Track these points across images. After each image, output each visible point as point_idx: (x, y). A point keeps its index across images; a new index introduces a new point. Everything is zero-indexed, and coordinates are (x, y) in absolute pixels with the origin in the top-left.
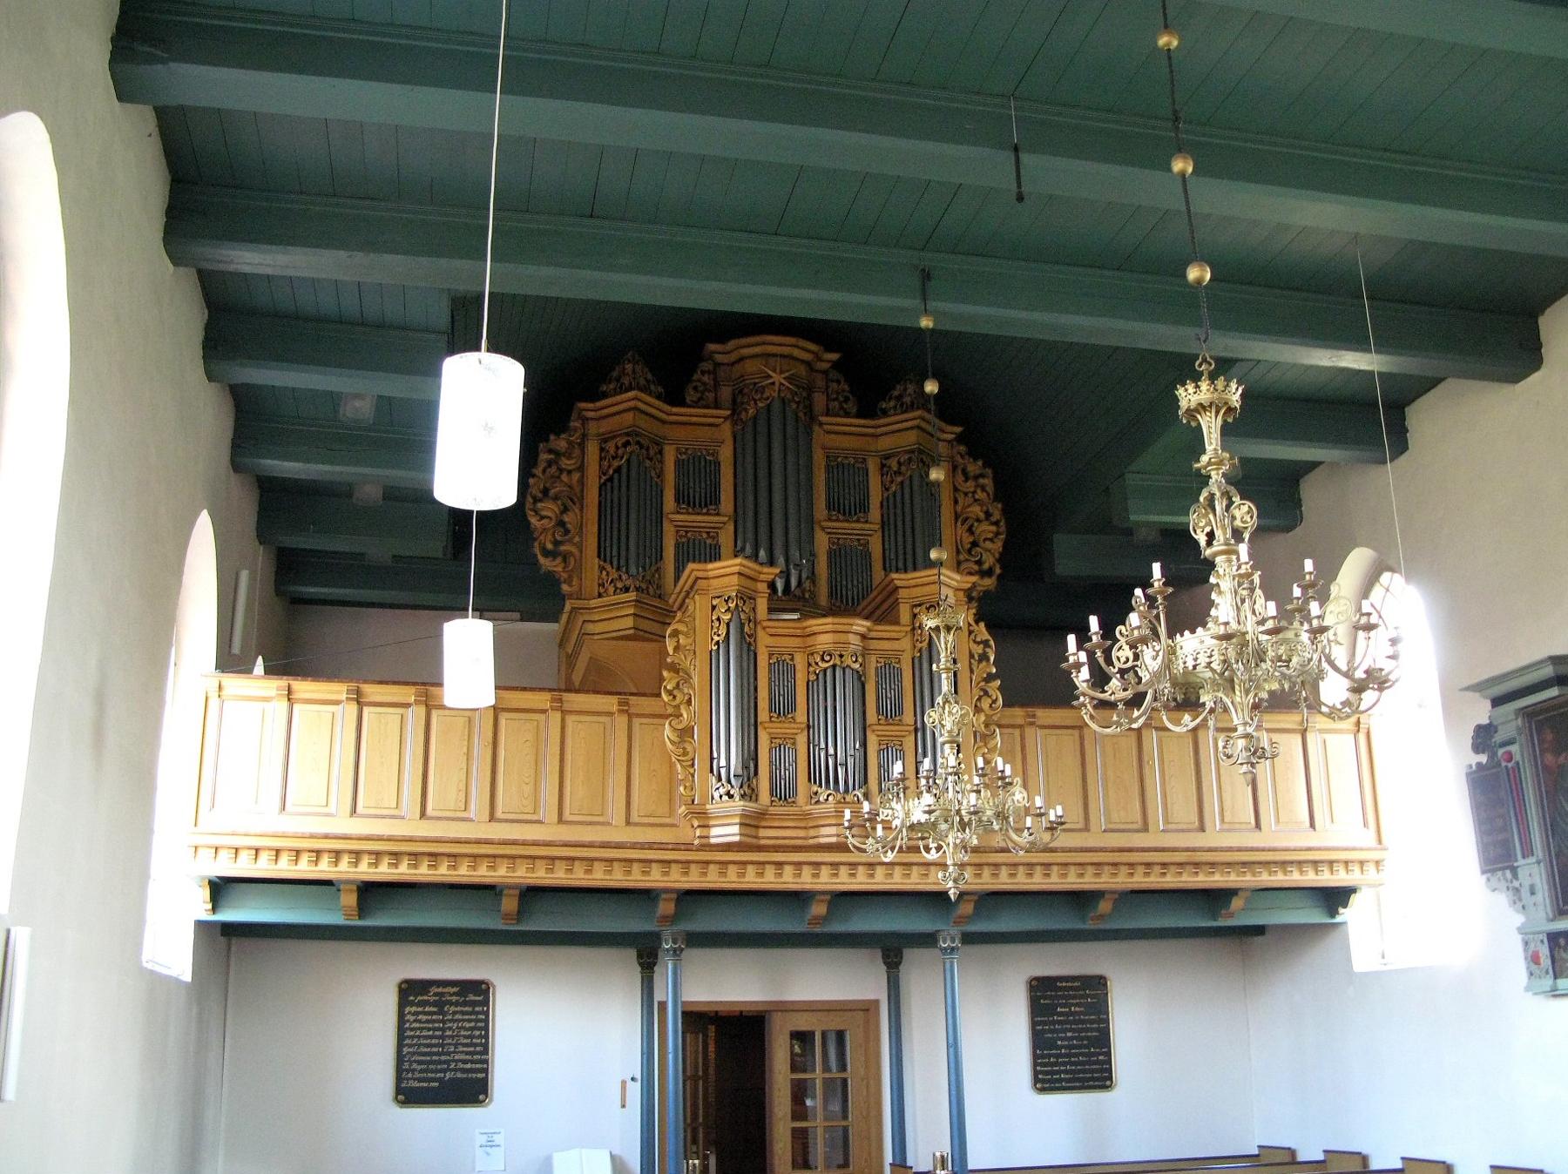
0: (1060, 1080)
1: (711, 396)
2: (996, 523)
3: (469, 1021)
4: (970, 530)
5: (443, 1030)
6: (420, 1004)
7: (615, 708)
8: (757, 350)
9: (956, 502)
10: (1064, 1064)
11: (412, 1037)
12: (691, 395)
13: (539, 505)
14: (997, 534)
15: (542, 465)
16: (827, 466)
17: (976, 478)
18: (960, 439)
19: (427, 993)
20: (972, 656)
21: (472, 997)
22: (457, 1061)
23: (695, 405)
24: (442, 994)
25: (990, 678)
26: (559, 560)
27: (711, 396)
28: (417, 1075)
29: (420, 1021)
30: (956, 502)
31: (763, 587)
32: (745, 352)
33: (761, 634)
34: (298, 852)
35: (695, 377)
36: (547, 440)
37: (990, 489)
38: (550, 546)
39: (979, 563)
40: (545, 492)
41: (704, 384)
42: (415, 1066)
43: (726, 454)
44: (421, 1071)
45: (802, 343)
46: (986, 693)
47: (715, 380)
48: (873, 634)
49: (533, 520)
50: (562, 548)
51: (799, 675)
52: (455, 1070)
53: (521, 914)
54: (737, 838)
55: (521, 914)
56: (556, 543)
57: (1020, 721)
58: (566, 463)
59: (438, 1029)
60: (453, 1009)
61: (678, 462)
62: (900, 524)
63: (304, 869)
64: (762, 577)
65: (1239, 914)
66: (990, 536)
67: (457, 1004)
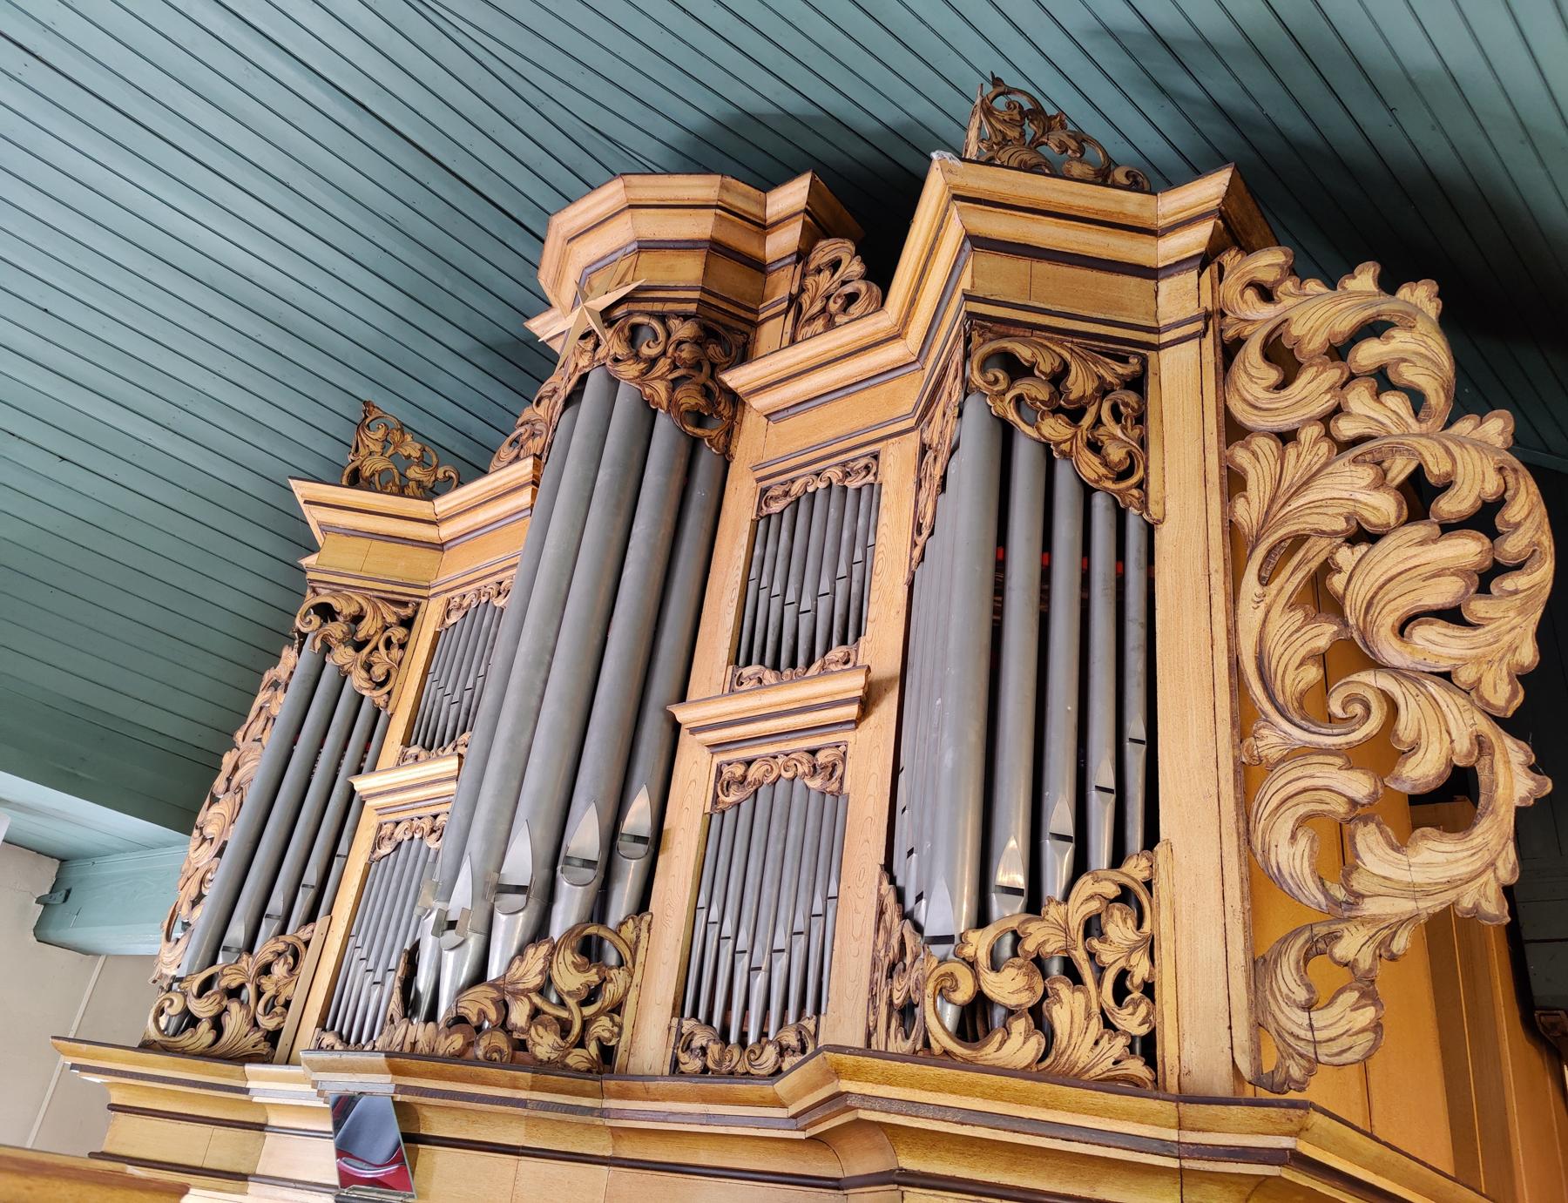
4: (1319, 596)
9: (1234, 482)
14: (1486, 578)
17: (1338, 351)
30: (1234, 482)
39: (1383, 753)
62: (393, 885)
66: (1443, 593)
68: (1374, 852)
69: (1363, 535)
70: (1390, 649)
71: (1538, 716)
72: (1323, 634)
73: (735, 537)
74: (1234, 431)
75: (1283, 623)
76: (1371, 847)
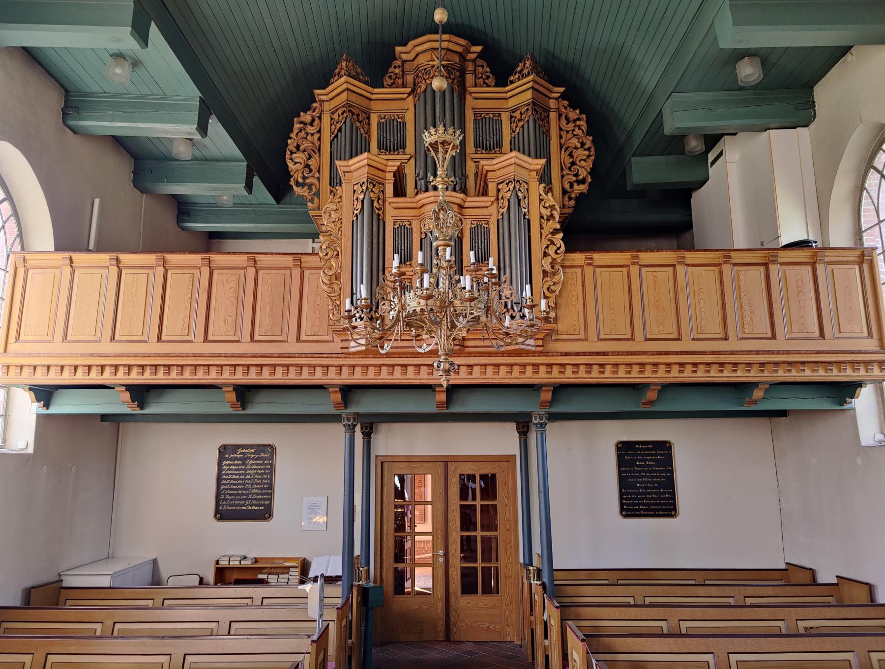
0: (639, 510)
1: (400, 81)
2: (589, 149)
3: (261, 469)
4: (571, 155)
5: (245, 475)
6: (231, 459)
7: (291, 264)
8: (425, 46)
9: (561, 137)
10: (642, 499)
11: (226, 480)
12: (387, 81)
13: (294, 155)
14: (589, 156)
15: (296, 131)
16: (475, 120)
17: (574, 121)
18: (563, 96)
19: (235, 453)
20: (542, 217)
21: (262, 455)
22: (253, 494)
23: (390, 86)
24: (244, 454)
25: (555, 232)
26: (306, 188)
27: (400, 81)
28: (229, 502)
29: (231, 470)
30: (561, 137)
31: (390, 176)
32: (419, 49)
34: (90, 367)
35: (391, 70)
36: (299, 116)
37: (584, 128)
38: (300, 180)
39: (576, 175)
40: (298, 147)
42: (227, 497)
43: (409, 117)
44: (231, 500)
46: (552, 243)
47: (403, 71)
48: (467, 205)
49: (290, 165)
50: (308, 181)
51: (414, 235)
52: (252, 499)
53: (449, 402)
55: (449, 402)
56: (304, 178)
57: (582, 263)
58: (310, 129)
59: (242, 474)
60: (251, 462)
61: (379, 124)
63: (94, 378)
65: (760, 400)
66: (584, 157)
67: (254, 459)
68: (575, 186)
69: (576, 148)
70: (578, 163)
71: (592, 172)
72: (571, 160)
74: (561, 129)
75: (567, 158)
76: (575, 185)
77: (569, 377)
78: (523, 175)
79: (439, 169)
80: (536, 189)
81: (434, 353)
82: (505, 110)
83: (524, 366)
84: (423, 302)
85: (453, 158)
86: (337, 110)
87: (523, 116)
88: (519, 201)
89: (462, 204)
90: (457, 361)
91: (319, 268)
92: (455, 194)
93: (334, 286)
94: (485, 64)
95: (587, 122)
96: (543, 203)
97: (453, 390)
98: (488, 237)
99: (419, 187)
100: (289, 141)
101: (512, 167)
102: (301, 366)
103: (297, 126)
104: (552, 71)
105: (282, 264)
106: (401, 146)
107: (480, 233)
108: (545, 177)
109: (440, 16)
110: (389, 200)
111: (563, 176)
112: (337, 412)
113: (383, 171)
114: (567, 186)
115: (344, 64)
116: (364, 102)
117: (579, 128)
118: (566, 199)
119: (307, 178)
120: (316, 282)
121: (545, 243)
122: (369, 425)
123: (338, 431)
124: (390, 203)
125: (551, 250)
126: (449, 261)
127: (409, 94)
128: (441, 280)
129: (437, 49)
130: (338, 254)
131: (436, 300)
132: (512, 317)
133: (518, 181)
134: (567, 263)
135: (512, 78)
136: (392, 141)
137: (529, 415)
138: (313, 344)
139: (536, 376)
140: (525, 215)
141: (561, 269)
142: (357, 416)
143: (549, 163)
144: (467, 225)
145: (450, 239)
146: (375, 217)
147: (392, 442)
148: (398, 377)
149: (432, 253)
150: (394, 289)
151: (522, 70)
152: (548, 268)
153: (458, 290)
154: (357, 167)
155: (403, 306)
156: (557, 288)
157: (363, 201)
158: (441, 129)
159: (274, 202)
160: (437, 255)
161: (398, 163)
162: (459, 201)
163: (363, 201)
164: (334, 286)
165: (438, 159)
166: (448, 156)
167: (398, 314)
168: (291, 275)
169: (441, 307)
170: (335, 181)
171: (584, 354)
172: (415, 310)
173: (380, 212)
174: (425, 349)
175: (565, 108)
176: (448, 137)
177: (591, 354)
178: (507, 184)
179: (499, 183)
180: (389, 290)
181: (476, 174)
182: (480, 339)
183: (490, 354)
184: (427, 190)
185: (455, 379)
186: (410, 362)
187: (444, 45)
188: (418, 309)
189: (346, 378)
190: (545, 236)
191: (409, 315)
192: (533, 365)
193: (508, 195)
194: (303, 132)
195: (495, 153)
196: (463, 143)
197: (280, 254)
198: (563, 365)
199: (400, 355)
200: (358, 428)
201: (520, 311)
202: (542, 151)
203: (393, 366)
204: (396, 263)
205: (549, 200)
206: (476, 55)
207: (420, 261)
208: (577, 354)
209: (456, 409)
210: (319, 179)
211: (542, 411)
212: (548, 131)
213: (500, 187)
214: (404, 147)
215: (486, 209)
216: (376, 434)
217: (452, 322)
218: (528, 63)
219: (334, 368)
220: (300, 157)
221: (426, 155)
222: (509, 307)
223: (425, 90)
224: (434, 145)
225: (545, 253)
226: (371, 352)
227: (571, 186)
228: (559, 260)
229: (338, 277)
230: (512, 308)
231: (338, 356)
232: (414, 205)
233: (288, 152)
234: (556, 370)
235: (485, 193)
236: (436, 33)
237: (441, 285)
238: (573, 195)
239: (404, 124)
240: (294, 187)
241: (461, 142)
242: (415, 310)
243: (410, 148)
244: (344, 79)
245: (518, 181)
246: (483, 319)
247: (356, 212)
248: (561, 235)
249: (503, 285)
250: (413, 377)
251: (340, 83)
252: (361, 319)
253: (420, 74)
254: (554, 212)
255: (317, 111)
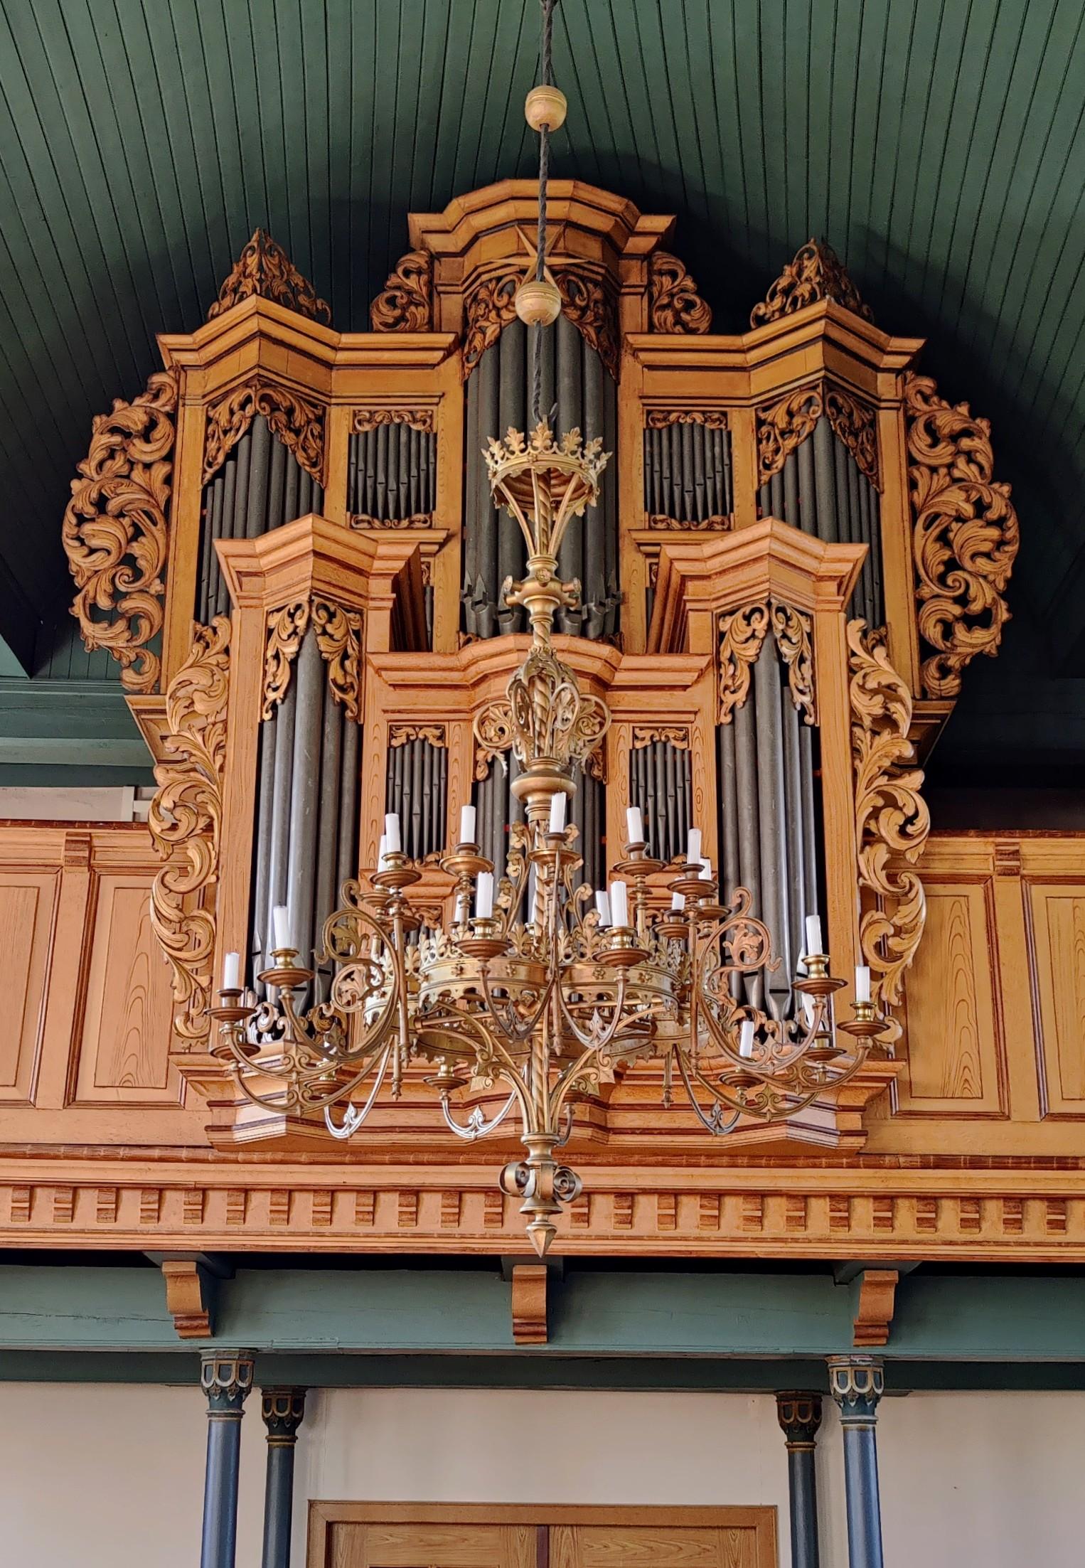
1: (421, 313)
2: (1000, 523)
4: (944, 539)
7: (60, 855)
9: (913, 485)
12: (382, 312)
13: (87, 528)
14: (1000, 544)
15: (97, 454)
16: (649, 430)
17: (955, 438)
18: (919, 364)
23: (391, 327)
25: (899, 768)
26: (121, 625)
27: (421, 313)
30: (913, 485)
31: (381, 589)
33: (372, 682)
35: (393, 280)
36: (109, 411)
38: (104, 603)
39: (963, 600)
40: (101, 504)
41: (410, 293)
43: (447, 420)
45: (588, 192)
46: (891, 802)
47: (430, 283)
48: (620, 678)
49: (75, 555)
50: (126, 605)
51: (454, 770)
53: (556, 1314)
54: (280, 1128)
55: (556, 1314)
56: (116, 596)
57: (987, 867)
58: (140, 450)
61: (354, 438)
64: (378, 565)
66: (986, 547)
69: (960, 519)
70: (967, 564)
72: (946, 554)
73: (633, 436)
74: (912, 461)
75: (932, 547)
76: (960, 630)
77: (949, 1238)
78: (796, 590)
79: (532, 555)
80: (838, 634)
81: (504, 1149)
82: (742, 401)
83: (803, 1198)
84: (472, 965)
85: (580, 524)
86: (225, 396)
87: (797, 421)
88: (784, 669)
89: (606, 675)
90: (586, 1177)
91: (149, 870)
92: (582, 645)
93: (194, 926)
94: (680, 268)
95: (992, 440)
96: (858, 678)
97: (570, 1276)
98: (688, 779)
99: (471, 628)
100: (76, 485)
101: (761, 569)
102: (75, 1188)
103: (101, 441)
104: (883, 288)
105: (32, 855)
106: (420, 502)
107: (659, 774)
108: (865, 600)
109: (543, 108)
110: (377, 661)
111: (919, 603)
112: (186, 1346)
113: (360, 572)
114: (934, 633)
115: (252, 261)
116: (311, 374)
117: (970, 459)
118: (933, 670)
119: (125, 595)
120: (138, 915)
121: (868, 801)
122: (291, 1392)
123: (186, 1413)
124: (379, 670)
125: (888, 825)
126: (561, 837)
127: (449, 352)
128: (534, 901)
129: (533, 221)
130: (209, 828)
131: (515, 962)
132: (761, 1035)
133: (781, 610)
134: (939, 868)
135: (761, 309)
136: (394, 484)
137: (818, 1367)
138: (117, 1114)
139: (842, 1233)
140: (803, 712)
141: (919, 885)
142: (253, 1361)
143: (875, 558)
144: (621, 745)
145: (566, 772)
146: (332, 711)
147: (370, 1453)
148: (387, 1230)
149: (508, 814)
150: (383, 925)
151: (792, 286)
152: (878, 882)
153: (588, 932)
154: (280, 561)
155: (409, 981)
156: (909, 946)
157: (294, 664)
158: (541, 435)
159: (24, 674)
160: (525, 819)
161: (409, 551)
162: (595, 667)
163: (294, 664)
164: (194, 926)
165: (530, 525)
166: (561, 519)
167: (392, 1009)
168: (59, 887)
169: (532, 984)
170: (211, 601)
171: (1000, 1163)
172: (445, 994)
173: (350, 697)
174: (475, 1126)
175: (926, 399)
176: (563, 460)
177: (1020, 1163)
178: (747, 618)
179: (723, 615)
180: (364, 927)
181: (651, 591)
182: (659, 1107)
183: (689, 1158)
184: (496, 632)
185: (576, 1239)
186: (429, 1180)
187: (556, 210)
188: (457, 990)
189: (221, 1230)
190: (870, 785)
191: (425, 1014)
192: (833, 1196)
193: (751, 650)
194: (120, 459)
195: (710, 528)
196: (610, 479)
197: (26, 823)
198: (930, 1200)
199: (399, 1155)
200: (253, 1403)
201: (790, 1016)
202: (854, 518)
203: (375, 1192)
204: (390, 842)
205: (877, 668)
206: (653, 241)
207: (467, 836)
208: (976, 1163)
209: (581, 1341)
210: (161, 598)
211: (865, 1354)
212: (873, 466)
213: (724, 626)
214: (427, 504)
215: (682, 694)
216: (312, 1425)
217: (566, 1027)
218: (810, 267)
219: (181, 1196)
220: (105, 533)
221: (496, 515)
222: (754, 1001)
223: (498, 341)
224: (519, 484)
225: (867, 832)
226: (305, 1136)
227: (948, 633)
228: (912, 857)
229: (207, 901)
230: (764, 1006)
231: (196, 1154)
232: (455, 677)
233: (70, 518)
234: (906, 1215)
235: (677, 644)
236: (534, 175)
237: (533, 915)
238: (953, 661)
239: (432, 437)
240: (84, 622)
241: (603, 476)
242: (445, 994)
243: (447, 509)
244: (251, 302)
245: (781, 610)
246: (668, 1028)
247: (271, 696)
248: (918, 778)
249: (733, 920)
250: (437, 1228)
251: (240, 315)
252: (276, 1033)
253: (483, 294)
254: (895, 707)
255: (164, 398)
